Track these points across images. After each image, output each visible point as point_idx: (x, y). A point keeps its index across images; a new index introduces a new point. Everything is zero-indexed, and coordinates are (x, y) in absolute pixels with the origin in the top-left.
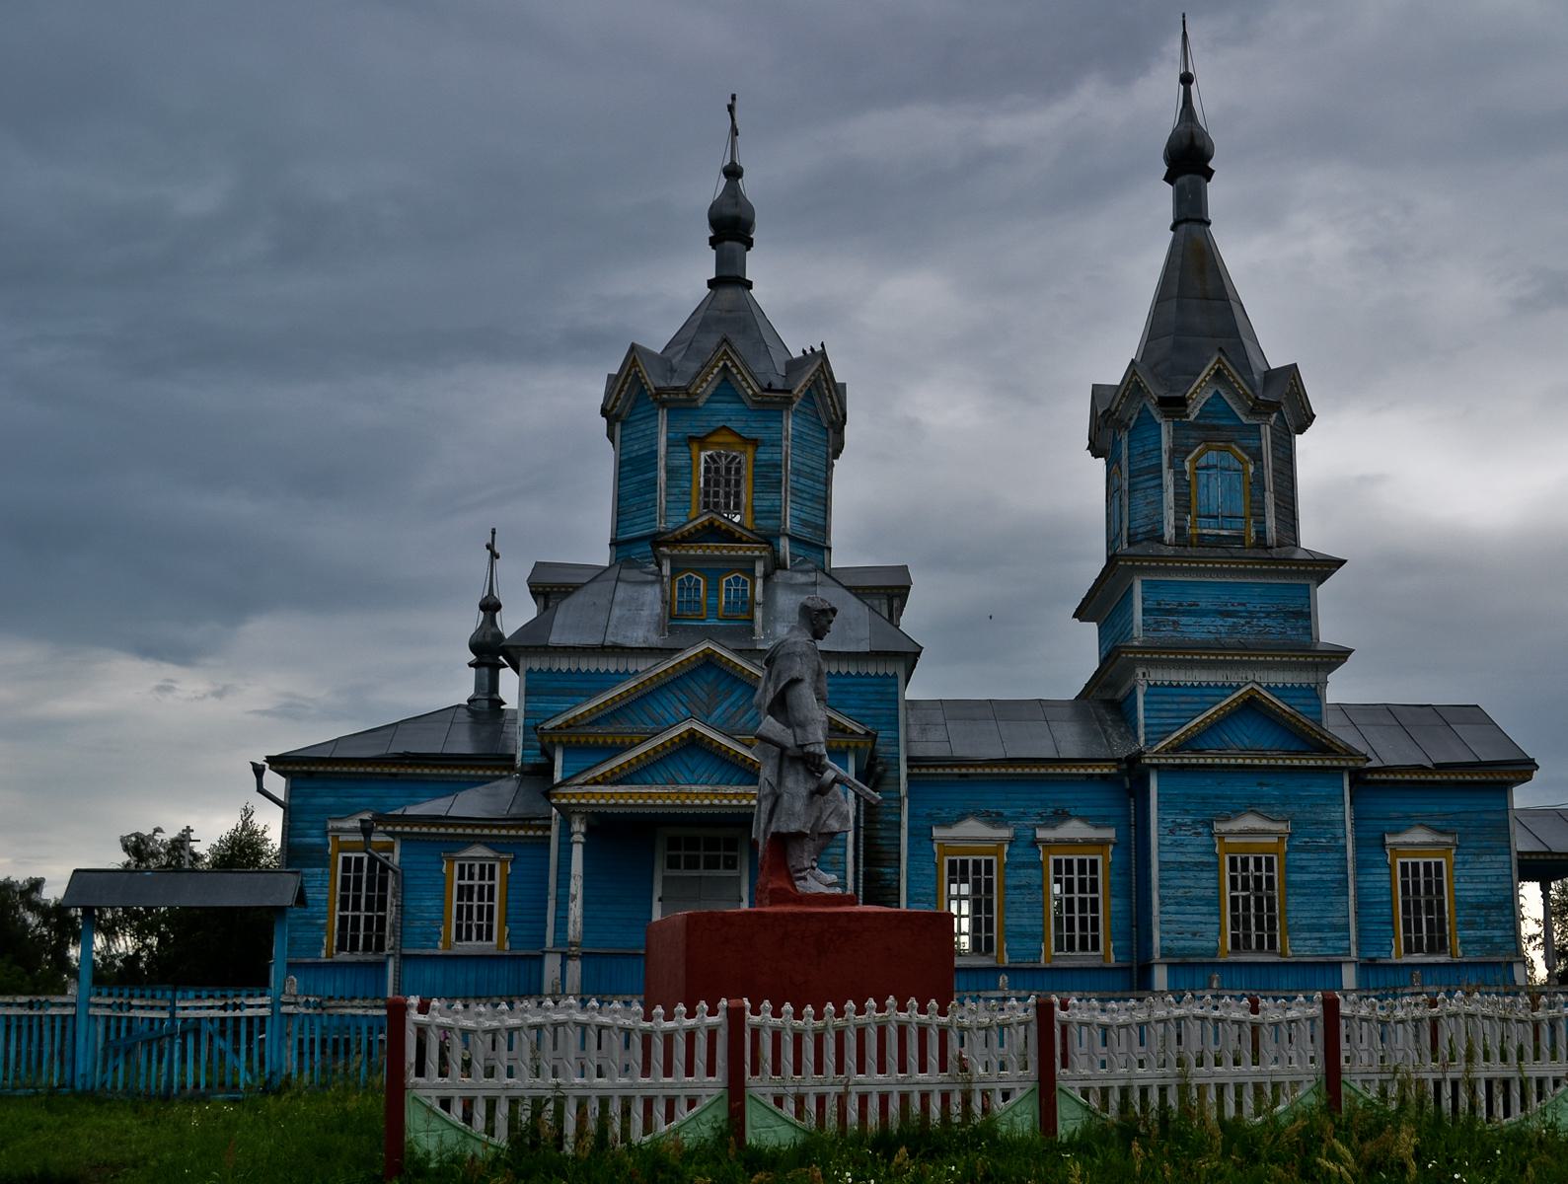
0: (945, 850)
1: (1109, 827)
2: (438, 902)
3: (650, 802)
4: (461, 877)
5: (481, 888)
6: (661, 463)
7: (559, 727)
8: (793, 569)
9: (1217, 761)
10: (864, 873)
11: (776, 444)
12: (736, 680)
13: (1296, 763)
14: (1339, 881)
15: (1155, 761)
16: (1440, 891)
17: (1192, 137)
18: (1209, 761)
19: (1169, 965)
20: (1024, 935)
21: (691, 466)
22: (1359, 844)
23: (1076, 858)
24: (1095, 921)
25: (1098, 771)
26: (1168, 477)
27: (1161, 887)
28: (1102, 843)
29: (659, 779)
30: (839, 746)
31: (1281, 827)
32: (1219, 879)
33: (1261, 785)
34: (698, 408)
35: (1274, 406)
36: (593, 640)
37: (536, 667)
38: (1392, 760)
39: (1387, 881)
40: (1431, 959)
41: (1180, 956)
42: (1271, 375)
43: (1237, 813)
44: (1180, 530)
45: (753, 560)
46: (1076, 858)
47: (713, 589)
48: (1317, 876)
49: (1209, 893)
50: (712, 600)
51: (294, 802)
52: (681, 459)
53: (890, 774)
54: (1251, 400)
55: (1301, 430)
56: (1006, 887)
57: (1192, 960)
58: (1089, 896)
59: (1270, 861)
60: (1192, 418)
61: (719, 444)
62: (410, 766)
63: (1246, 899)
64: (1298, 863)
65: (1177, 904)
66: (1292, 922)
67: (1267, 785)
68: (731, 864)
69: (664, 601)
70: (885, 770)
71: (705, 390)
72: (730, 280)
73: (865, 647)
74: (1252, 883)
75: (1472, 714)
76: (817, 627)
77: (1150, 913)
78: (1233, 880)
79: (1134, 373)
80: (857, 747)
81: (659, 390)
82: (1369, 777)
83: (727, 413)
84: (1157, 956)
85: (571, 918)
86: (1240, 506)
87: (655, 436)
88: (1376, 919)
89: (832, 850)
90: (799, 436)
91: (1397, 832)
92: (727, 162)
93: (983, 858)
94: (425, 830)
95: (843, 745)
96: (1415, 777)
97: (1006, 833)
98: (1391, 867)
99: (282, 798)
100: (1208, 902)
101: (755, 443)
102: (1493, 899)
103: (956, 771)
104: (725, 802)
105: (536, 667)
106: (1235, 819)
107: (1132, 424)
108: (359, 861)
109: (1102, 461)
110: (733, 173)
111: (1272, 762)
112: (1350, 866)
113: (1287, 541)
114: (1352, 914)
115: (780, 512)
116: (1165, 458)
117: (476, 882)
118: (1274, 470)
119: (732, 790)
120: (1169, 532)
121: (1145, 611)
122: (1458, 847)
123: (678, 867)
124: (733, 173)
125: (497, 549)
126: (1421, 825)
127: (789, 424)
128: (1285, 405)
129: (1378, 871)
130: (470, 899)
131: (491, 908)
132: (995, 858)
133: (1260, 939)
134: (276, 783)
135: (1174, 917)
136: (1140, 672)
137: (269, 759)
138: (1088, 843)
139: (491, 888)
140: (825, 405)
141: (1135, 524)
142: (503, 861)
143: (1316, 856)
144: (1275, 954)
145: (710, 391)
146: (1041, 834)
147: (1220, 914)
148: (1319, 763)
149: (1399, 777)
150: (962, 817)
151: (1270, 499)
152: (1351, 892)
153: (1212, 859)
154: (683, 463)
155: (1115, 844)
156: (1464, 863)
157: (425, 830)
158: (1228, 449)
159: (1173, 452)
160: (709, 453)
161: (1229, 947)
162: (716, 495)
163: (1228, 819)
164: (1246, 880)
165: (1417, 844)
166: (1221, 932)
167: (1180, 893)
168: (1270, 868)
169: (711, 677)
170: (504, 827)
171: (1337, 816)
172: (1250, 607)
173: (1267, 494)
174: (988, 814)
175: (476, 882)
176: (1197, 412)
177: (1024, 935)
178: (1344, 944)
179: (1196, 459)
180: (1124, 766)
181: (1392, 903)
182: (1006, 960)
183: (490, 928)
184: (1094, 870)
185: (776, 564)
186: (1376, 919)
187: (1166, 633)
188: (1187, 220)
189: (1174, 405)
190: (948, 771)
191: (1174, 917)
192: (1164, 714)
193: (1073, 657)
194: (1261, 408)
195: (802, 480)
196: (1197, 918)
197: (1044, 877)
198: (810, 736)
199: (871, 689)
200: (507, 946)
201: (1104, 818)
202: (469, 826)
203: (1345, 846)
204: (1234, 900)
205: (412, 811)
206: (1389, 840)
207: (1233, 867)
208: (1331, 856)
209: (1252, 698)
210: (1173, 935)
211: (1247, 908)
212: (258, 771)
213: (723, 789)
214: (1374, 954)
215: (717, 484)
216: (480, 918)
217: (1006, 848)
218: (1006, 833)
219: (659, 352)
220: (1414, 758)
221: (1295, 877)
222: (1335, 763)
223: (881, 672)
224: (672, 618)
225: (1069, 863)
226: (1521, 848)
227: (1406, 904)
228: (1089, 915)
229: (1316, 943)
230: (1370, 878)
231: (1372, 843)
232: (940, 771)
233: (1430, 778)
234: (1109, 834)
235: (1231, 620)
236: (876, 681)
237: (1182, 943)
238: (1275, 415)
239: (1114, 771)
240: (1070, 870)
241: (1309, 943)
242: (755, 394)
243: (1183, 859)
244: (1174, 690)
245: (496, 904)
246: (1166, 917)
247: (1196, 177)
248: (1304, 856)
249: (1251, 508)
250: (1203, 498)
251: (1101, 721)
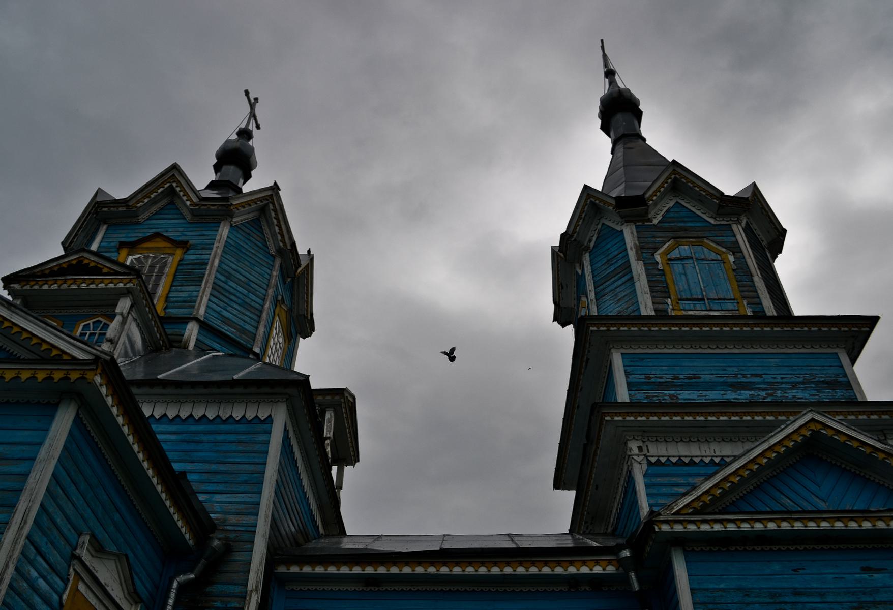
26: (638, 268)
33: (866, 570)
34: (138, 223)
53: (239, 556)
54: (717, 198)
61: (147, 248)
67: (878, 571)
86: (728, 289)
101: (184, 245)
107: (592, 245)
109: (570, 329)
115: (195, 302)
116: (632, 254)
127: (224, 231)
158: (701, 244)
160: (137, 256)
172: (769, 379)
176: (659, 217)
199: (232, 437)
223: (250, 415)
239: (611, 569)
242: (193, 204)
249: (741, 292)
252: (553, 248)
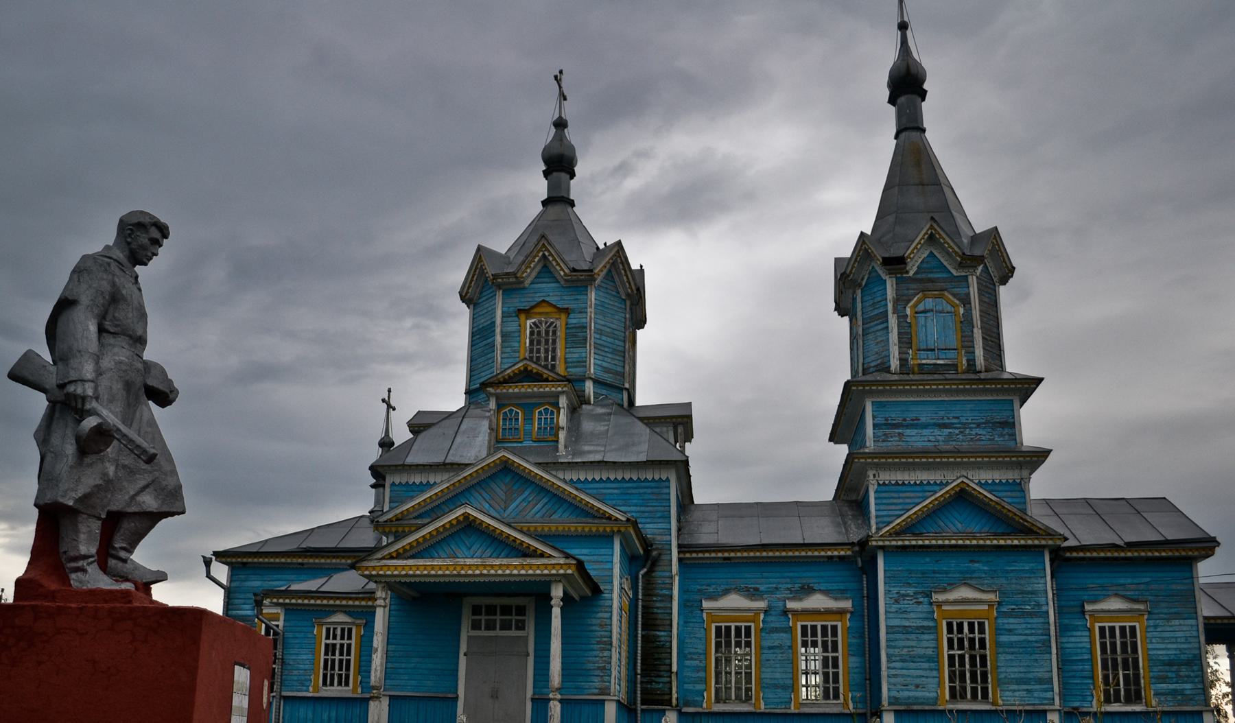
0: (713, 616)
1: (847, 598)
2: (310, 657)
3: (433, 572)
4: (328, 638)
5: (342, 645)
6: (498, 330)
7: (391, 520)
8: (596, 404)
9: (934, 542)
10: (643, 636)
11: (583, 311)
12: (527, 480)
13: (1002, 542)
14: (1043, 642)
15: (881, 543)
16: (1135, 650)
17: (908, 66)
18: (927, 542)
19: (895, 711)
20: (776, 686)
21: (520, 330)
22: (1060, 612)
23: (819, 624)
24: (836, 675)
25: (836, 553)
26: (893, 321)
27: (888, 647)
28: (841, 612)
29: (443, 554)
30: (605, 531)
31: (991, 597)
32: (938, 640)
33: (972, 561)
34: (525, 288)
35: (980, 260)
36: (439, 459)
37: (397, 482)
38: (1088, 540)
39: (1086, 642)
40: (1129, 708)
41: (906, 704)
42: (976, 238)
43: (952, 586)
44: (903, 361)
45: (557, 396)
46: (819, 624)
47: (529, 418)
48: (1024, 638)
49: (929, 652)
50: (528, 427)
51: (234, 584)
52: (512, 326)
53: (663, 557)
55: (1004, 281)
56: (762, 648)
57: (915, 707)
58: (830, 655)
59: (981, 625)
60: (911, 273)
61: (540, 314)
62: (311, 557)
63: (962, 657)
64: (1007, 627)
65: (902, 661)
66: (1002, 676)
68: (521, 626)
69: (491, 429)
70: (660, 555)
71: (529, 275)
72: (558, 200)
73: (643, 458)
74: (966, 644)
75: (1162, 503)
76: (134, 246)
77: (879, 669)
78: (950, 641)
79: (864, 242)
80: (619, 531)
81: (495, 276)
82: (1068, 555)
83: (549, 291)
84: (885, 702)
85: (373, 667)
86: (953, 340)
87: (494, 311)
88: (1078, 674)
89: (600, 615)
90: (601, 306)
91: (1095, 602)
92: (557, 116)
93: (743, 624)
94: (300, 601)
95: (608, 530)
96: (1109, 554)
97: (762, 604)
99: (224, 581)
100: (929, 659)
102: (1183, 657)
103: (720, 555)
104: (492, 572)
105: (397, 482)
106: (951, 590)
110: (560, 124)
111: (981, 542)
112: (1052, 628)
113: (994, 367)
114: (1055, 670)
117: (338, 641)
118: (981, 311)
119: (498, 562)
120: (894, 364)
121: (875, 426)
122: (1149, 613)
123: (480, 629)
124: (560, 124)
125: (393, 403)
126: (1116, 595)
127: (592, 296)
128: (989, 261)
129: (1079, 633)
130: (334, 654)
131: (348, 661)
132: (753, 625)
133: (974, 690)
134: (221, 571)
135: (899, 672)
136: (871, 473)
137: (216, 554)
138: (829, 612)
139: (349, 646)
140: (623, 283)
141: (867, 360)
142: (358, 626)
143: (1022, 620)
144: (988, 703)
145: (534, 274)
146: (791, 605)
147: (939, 670)
148: (1023, 542)
149: (1095, 554)
150: (726, 592)
151: (978, 334)
152: (1054, 651)
153: (931, 624)
154: (514, 329)
155: (852, 613)
156: (1156, 626)
157: (300, 601)
159: (897, 301)
161: (947, 697)
162: (538, 351)
163: (944, 590)
164: (961, 641)
165: (1114, 611)
166: (940, 684)
167: (905, 651)
168: (982, 631)
169: (508, 479)
170: (357, 599)
171: (1041, 587)
173: (975, 330)
175: (338, 641)
176: (915, 269)
177: (776, 686)
178: (1049, 695)
179: (916, 305)
180: (857, 548)
181: (1092, 661)
182: (763, 706)
183: (347, 677)
184: (835, 634)
185: (583, 400)
186: (1078, 674)
187: (893, 444)
188: (906, 129)
189: (895, 264)
190: (713, 555)
191: (899, 672)
192: (893, 507)
193: (820, 467)
194: (968, 261)
195: (604, 338)
197: (794, 640)
198: (72, 372)
199: (649, 491)
200: (359, 690)
201: (843, 591)
202: (332, 598)
203: (1047, 612)
204: (951, 658)
205: (294, 587)
206: (1088, 607)
207: (950, 630)
208: (1035, 620)
209: (962, 490)
210: (899, 687)
211: (962, 664)
212: (208, 563)
213: (490, 561)
214: (1076, 704)
215: (539, 343)
216: (340, 669)
217: (762, 616)
218: (762, 604)
219: (503, 252)
220: (1107, 538)
221: (1004, 638)
222: (1036, 542)
224: (498, 441)
225: (814, 628)
226: (1206, 613)
227: (1104, 662)
228: (831, 670)
230: (1073, 639)
231: (1072, 610)
232: (707, 555)
233: (1122, 554)
234: (847, 604)
235: (947, 431)
236: (653, 484)
237: (906, 694)
238: (980, 268)
239: (849, 553)
240: (814, 634)
241: (1017, 694)
242: (566, 275)
243: (907, 624)
244: (899, 488)
245: (352, 658)
246: (893, 672)
247: (914, 96)
248: (1011, 620)
250: (922, 335)
251: (842, 515)
252: (838, 261)
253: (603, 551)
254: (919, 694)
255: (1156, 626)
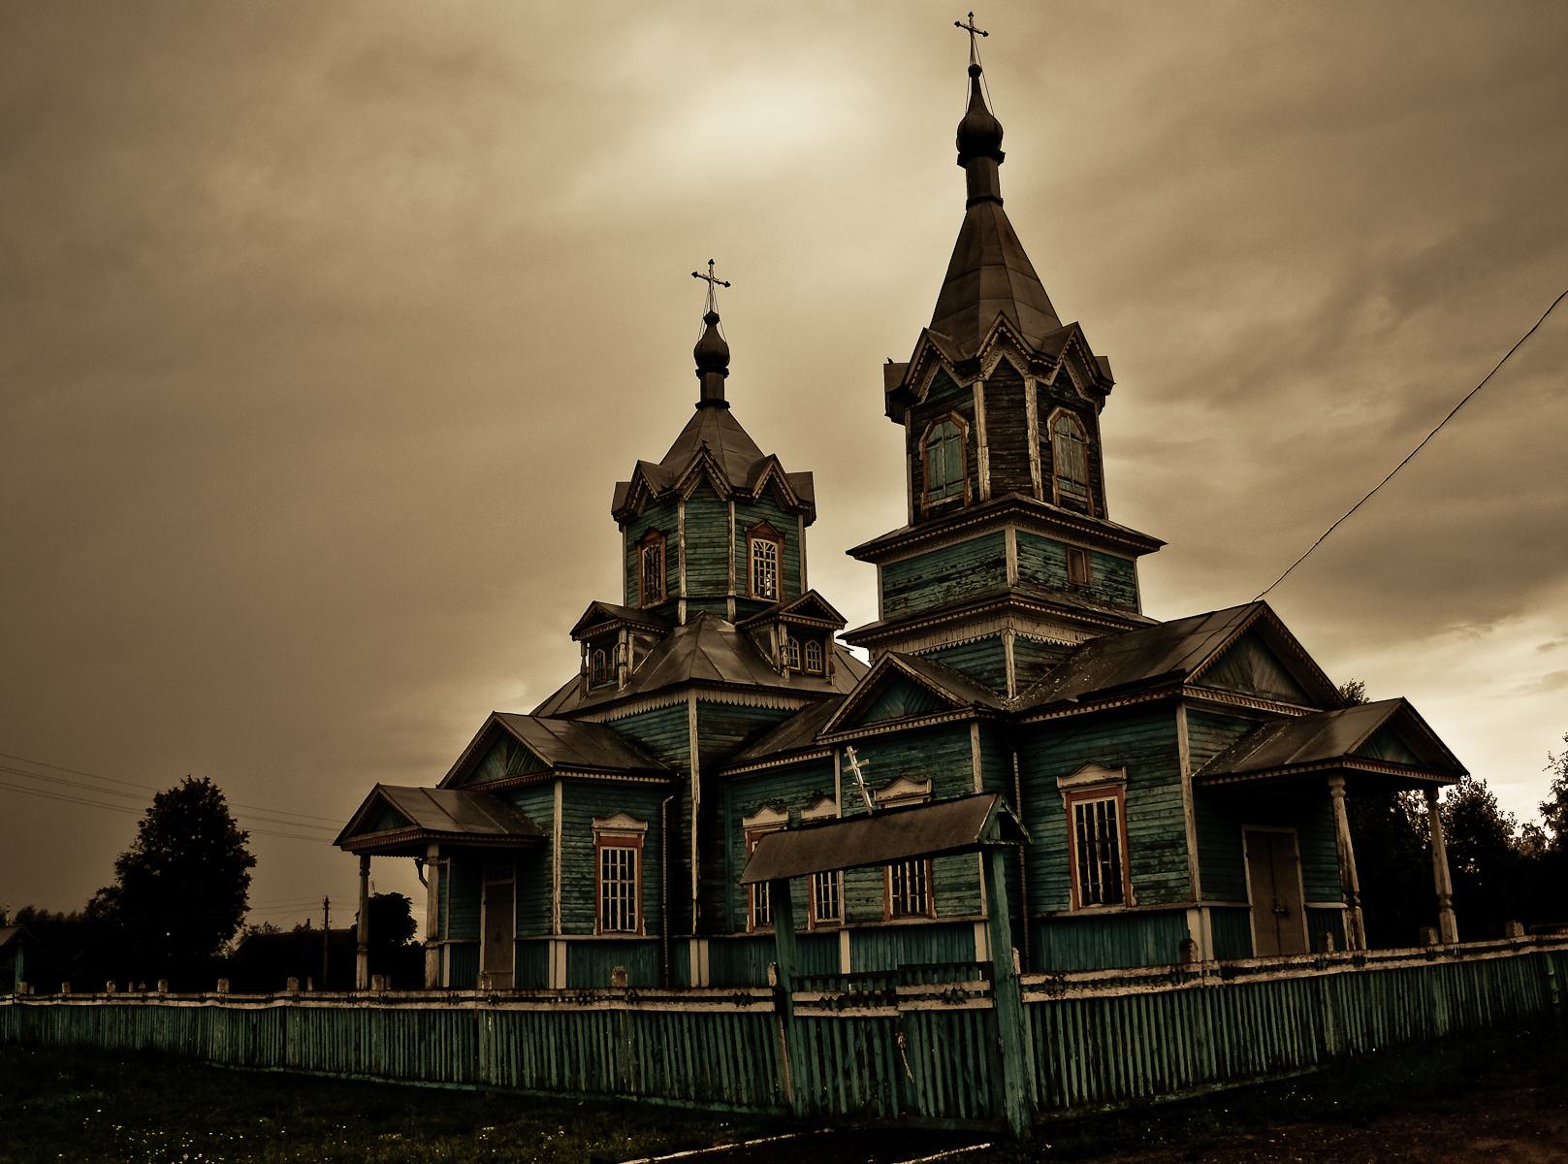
97: (785, 817)
98: (1068, 811)
102: (1167, 837)
108: (1089, 807)
110: (712, 319)
124: (712, 319)
127: (682, 513)
156: (1137, 798)
174: (775, 802)
196: (869, 884)
214: (1054, 908)
229: (955, 902)
230: (1050, 826)
237: (860, 909)
253: (1164, 732)
254: (869, 909)
255: (1137, 798)
